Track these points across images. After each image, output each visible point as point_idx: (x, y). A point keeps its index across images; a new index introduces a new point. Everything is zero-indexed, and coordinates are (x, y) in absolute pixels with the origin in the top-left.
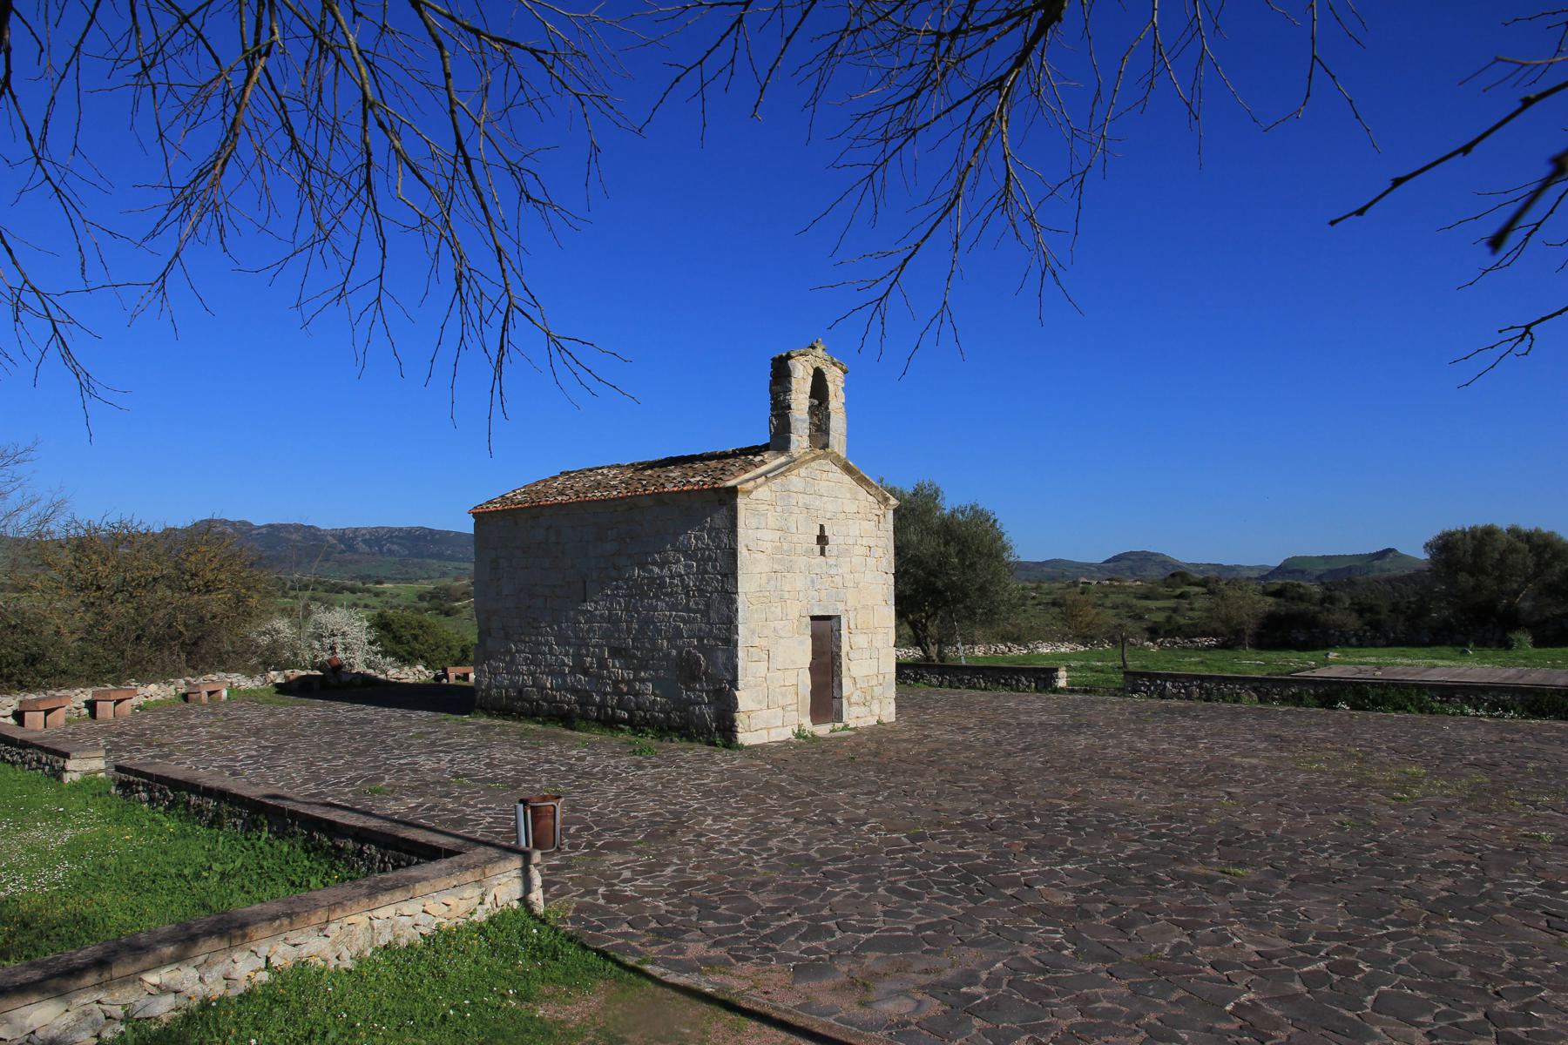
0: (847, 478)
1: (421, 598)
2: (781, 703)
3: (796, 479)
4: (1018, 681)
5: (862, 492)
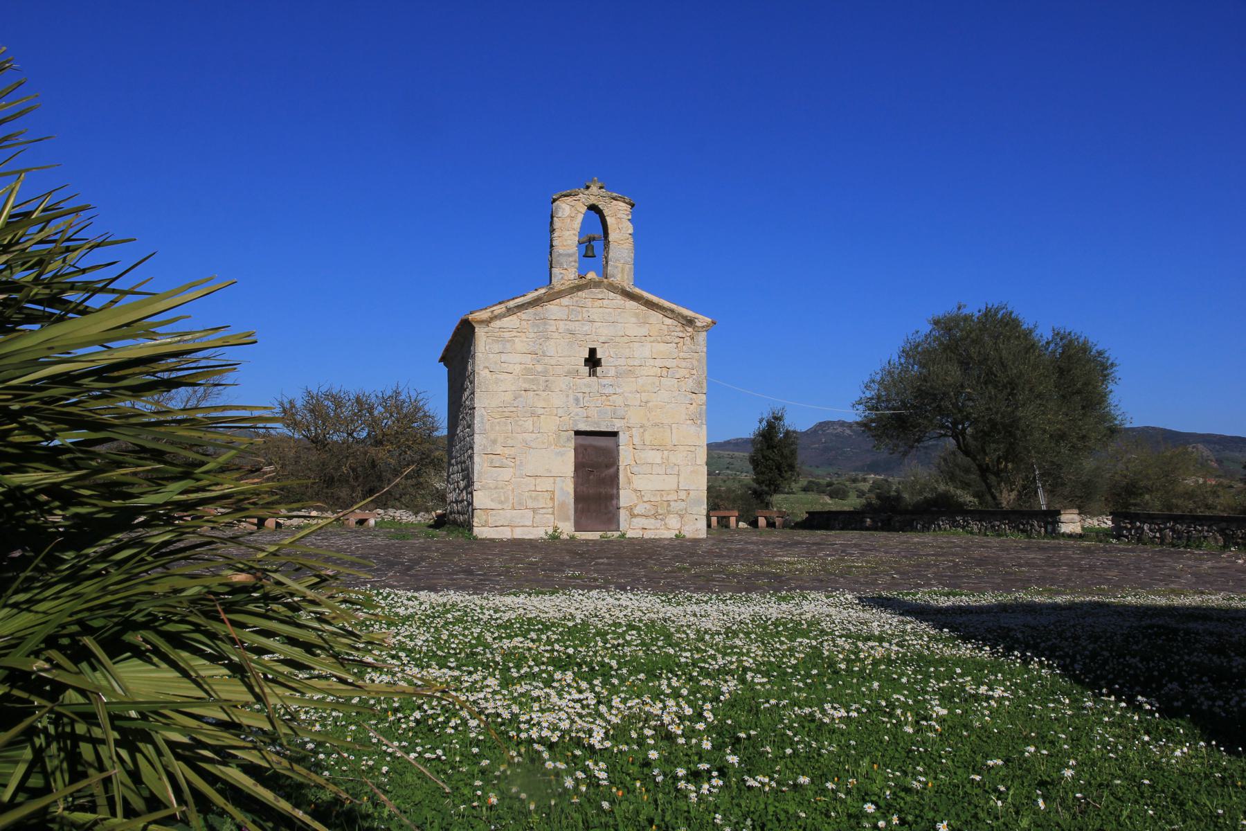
2: (531, 504)
3: (554, 309)
4: (1032, 525)
5: (655, 316)
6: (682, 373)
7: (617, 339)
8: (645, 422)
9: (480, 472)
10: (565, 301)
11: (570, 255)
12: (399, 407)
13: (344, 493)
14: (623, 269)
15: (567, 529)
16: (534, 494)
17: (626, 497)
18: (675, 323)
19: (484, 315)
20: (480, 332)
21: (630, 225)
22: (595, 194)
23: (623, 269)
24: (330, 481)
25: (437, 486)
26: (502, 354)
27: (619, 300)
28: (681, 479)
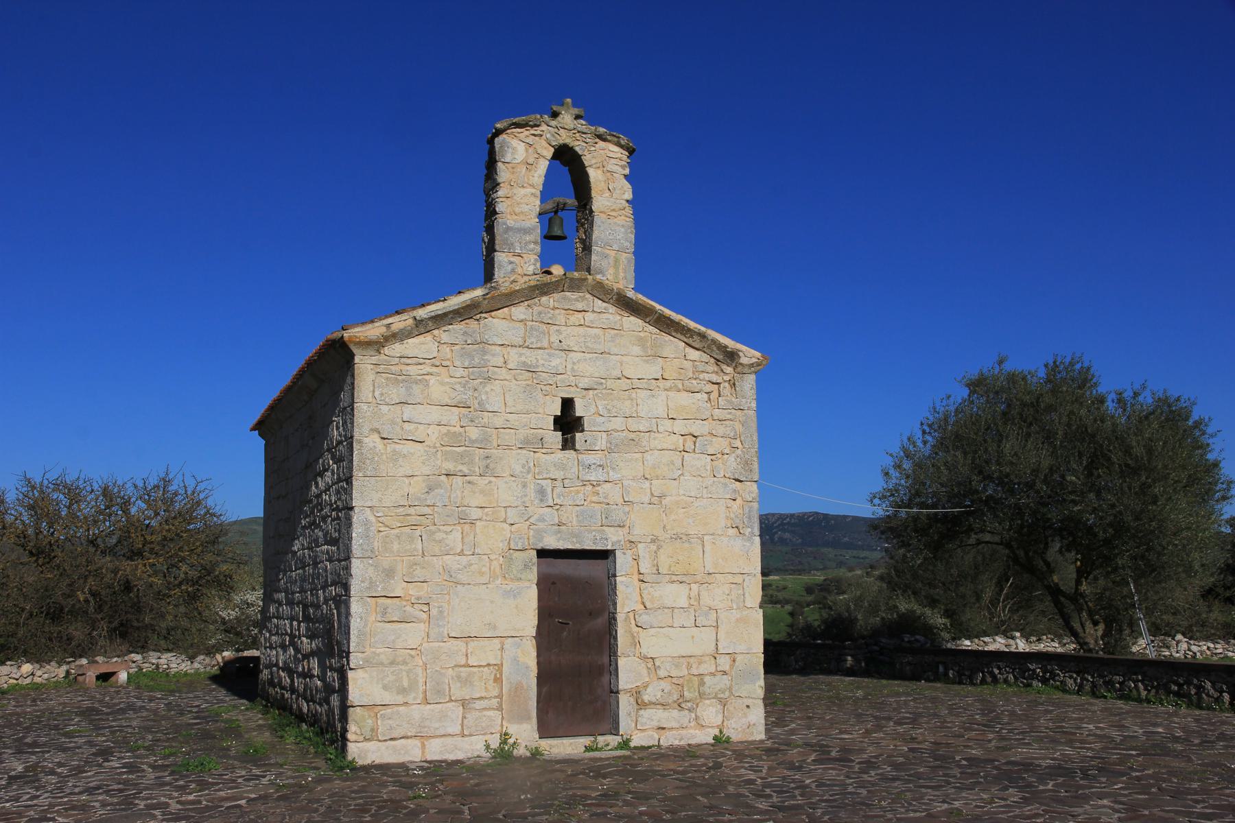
0: (633, 322)
1: (809, 590)
2: (458, 693)
3: (498, 325)
4: (1200, 688)
5: (673, 345)
6: (719, 444)
7: (610, 383)
8: (659, 532)
9: (361, 633)
10: (519, 311)
11: (526, 231)
12: (169, 502)
13: (77, 631)
14: (616, 261)
15: (525, 735)
16: (464, 671)
17: (629, 672)
18: (706, 357)
19: (374, 331)
20: (364, 363)
21: (627, 186)
22: (567, 127)
23: (616, 261)
24: (55, 615)
25: (224, 614)
26: (425, 407)
27: (612, 315)
28: (721, 635)
